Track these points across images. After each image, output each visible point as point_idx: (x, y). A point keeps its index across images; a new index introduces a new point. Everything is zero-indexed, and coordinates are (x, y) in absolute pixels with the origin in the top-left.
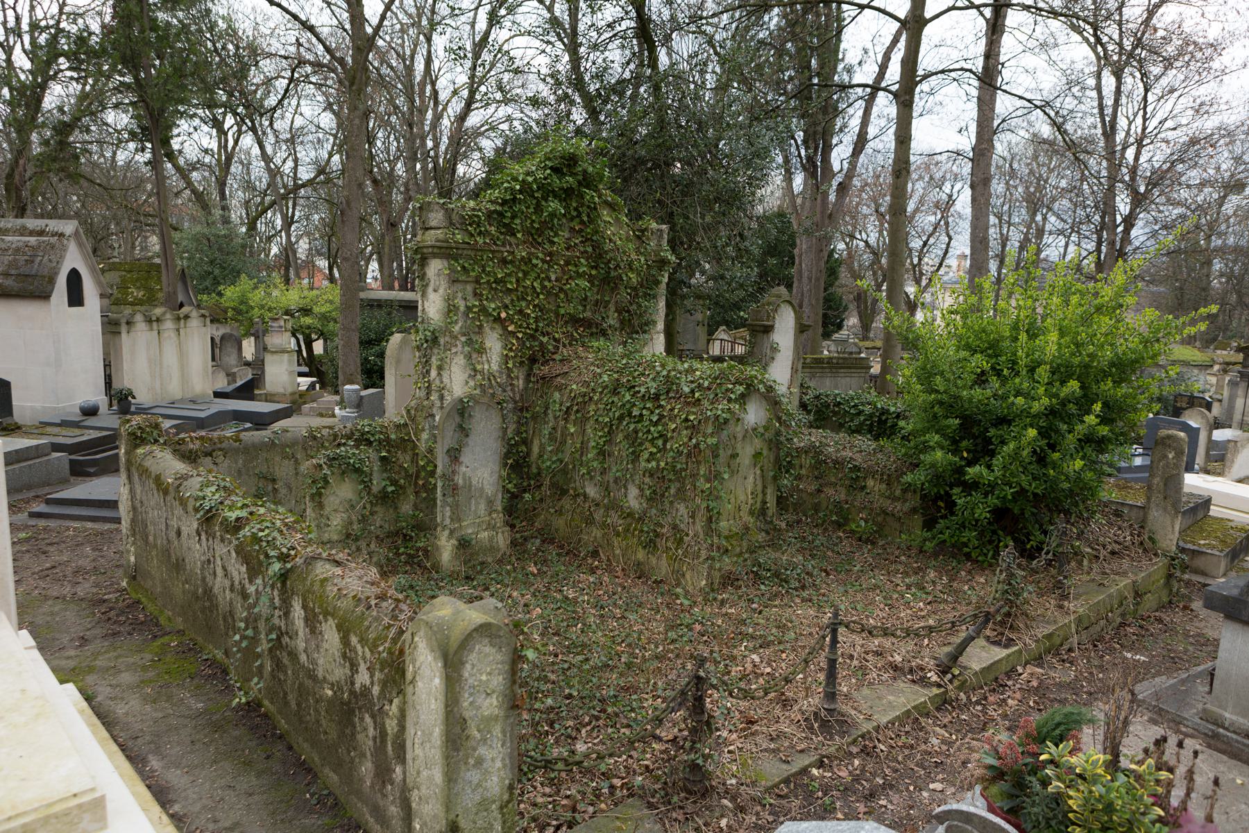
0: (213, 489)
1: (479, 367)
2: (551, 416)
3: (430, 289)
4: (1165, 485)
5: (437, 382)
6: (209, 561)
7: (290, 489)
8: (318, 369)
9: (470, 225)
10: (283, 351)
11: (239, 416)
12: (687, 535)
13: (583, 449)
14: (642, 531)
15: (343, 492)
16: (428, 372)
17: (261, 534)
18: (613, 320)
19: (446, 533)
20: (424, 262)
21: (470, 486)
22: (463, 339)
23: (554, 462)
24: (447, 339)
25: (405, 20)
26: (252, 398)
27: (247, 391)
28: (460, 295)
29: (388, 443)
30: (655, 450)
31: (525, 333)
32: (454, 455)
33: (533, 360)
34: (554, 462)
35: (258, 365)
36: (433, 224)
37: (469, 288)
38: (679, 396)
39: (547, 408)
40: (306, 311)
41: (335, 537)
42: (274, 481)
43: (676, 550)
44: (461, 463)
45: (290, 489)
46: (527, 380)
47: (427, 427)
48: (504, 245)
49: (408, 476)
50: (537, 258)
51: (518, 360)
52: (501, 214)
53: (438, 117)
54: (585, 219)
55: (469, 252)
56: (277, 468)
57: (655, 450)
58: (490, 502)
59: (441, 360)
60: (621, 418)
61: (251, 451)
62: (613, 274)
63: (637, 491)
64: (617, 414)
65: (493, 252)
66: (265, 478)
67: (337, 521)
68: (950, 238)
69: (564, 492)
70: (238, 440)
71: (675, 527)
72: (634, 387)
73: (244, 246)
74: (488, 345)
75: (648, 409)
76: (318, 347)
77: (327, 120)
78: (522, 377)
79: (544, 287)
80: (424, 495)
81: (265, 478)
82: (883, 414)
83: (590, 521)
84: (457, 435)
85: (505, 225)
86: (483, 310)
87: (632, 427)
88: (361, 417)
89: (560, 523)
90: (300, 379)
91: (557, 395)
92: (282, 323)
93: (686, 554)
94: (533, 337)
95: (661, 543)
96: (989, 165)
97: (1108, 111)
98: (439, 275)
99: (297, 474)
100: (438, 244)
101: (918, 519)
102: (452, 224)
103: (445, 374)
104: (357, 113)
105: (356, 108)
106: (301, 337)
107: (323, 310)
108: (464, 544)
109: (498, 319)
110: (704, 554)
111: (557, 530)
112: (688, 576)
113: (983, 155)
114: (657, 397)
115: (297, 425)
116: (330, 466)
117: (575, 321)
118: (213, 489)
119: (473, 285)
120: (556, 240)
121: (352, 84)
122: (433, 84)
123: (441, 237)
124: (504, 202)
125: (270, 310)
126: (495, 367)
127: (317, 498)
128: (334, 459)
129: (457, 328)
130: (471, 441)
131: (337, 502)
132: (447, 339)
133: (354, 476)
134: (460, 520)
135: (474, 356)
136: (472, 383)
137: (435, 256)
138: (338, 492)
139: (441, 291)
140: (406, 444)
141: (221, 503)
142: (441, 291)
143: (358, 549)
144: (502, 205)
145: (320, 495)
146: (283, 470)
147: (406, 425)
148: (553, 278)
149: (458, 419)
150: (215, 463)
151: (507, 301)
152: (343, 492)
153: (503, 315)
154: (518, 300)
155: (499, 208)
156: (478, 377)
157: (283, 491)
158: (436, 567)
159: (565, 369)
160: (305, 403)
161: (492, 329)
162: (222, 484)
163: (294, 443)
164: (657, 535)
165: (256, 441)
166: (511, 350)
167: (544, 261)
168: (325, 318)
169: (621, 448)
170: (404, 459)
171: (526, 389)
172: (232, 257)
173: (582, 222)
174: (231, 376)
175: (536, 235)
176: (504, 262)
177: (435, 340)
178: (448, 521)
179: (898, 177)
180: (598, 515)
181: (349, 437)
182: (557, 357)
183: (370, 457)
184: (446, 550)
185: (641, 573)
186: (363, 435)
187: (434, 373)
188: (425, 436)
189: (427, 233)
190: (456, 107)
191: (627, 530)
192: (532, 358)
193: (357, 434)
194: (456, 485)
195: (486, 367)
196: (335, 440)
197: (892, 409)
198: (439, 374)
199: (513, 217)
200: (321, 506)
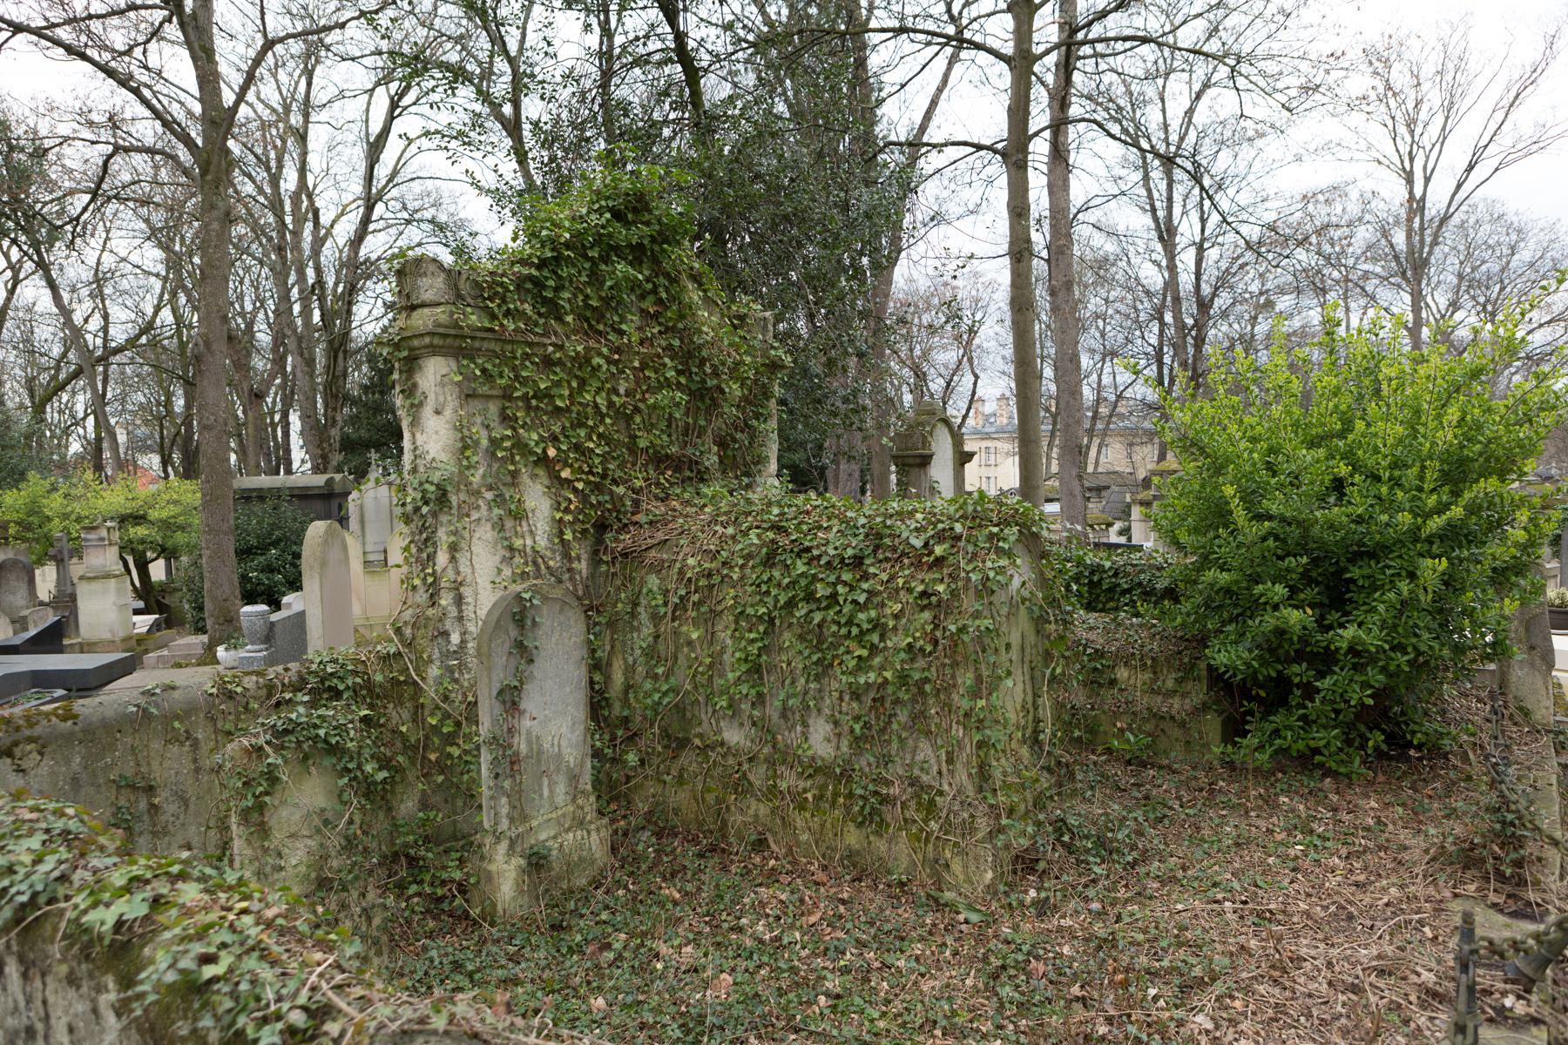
0: (35, 843)
1: (518, 543)
2: (644, 617)
3: (428, 411)
4: (1527, 630)
5: (451, 574)
6: (30, 1032)
7: (185, 802)
8: (158, 603)
9: (491, 299)
10: (107, 576)
11: (42, 680)
12: (941, 793)
13: (716, 665)
14: (850, 795)
15: (307, 796)
16: (431, 558)
17: (209, 971)
18: (711, 460)
19: (504, 846)
20: (412, 364)
21: (540, 752)
22: (489, 495)
23: (665, 694)
24: (463, 496)
25: (266, 114)
26: (60, 650)
27: (50, 640)
28: (479, 420)
30: (865, 653)
31: (587, 483)
32: (510, 699)
33: (602, 527)
34: (665, 694)
35: (66, 600)
36: (428, 296)
37: (493, 408)
38: (901, 554)
39: (636, 604)
40: (138, 519)
42: (150, 790)
43: (926, 821)
44: (522, 713)
45: (185, 802)
46: (595, 560)
47: (436, 655)
48: (546, 334)
49: (410, 748)
50: (600, 354)
51: (578, 527)
52: (539, 284)
53: (318, 243)
54: (664, 295)
55: (492, 346)
56: (155, 765)
57: (865, 653)
58: (574, 778)
59: (455, 533)
60: (791, 604)
61: (101, 735)
62: (710, 383)
63: (829, 727)
64: (782, 600)
65: (531, 345)
66: (133, 787)
67: (297, 857)
68: (977, 377)
69: (683, 743)
70: (69, 716)
71: (914, 781)
72: (808, 550)
73: (28, 437)
74: (530, 504)
75: (845, 583)
76: (157, 571)
77: (152, 257)
78: (584, 556)
79: (611, 404)
80: (440, 779)
81: (133, 787)
82: (1092, 573)
83: (741, 787)
84: (513, 662)
85: (546, 301)
86: (520, 446)
87: (818, 617)
88: (271, 661)
89: (680, 798)
90: (137, 618)
91: (653, 581)
92: (104, 533)
93: (947, 827)
94: (597, 488)
95: (892, 814)
96: (1070, 265)
97: (1161, 214)
98: (443, 385)
99: (197, 770)
100: (441, 330)
101: (1212, 724)
102: (459, 296)
103: (463, 559)
104: (215, 213)
105: (213, 207)
106: (130, 560)
107: (165, 514)
108: (536, 862)
109: (543, 460)
110: (983, 825)
111: (676, 812)
112: (956, 867)
113: (1062, 253)
114: (858, 561)
115: (124, 691)
116: (279, 749)
117: (659, 460)
118: (35, 843)
119: (499, 403)
120: (624, 327)
121: (204, 172)
122: (310, 196)
123: (443, 318)
124: (543, 264)
125: (79, 520)
126: (542, 542)
127: (255, 816)
128: (286, 732)
129: (476, 479)
130: (538, 669)
131: (297, 817)
132: (463, 496)
133: (328, 761)
134: (525, 818)
135: (509, 524)
136: (507, 572)
137: (434, 351)
139: (448, 412)
140: (403, 689)
141: (63, 878)
142: (448, 412)
143: (343, 906)
144: (538, 267)
145: (260, 807)
146: (168, 765)
148: (622, 391)
149: (514, 633)
150: (20, 770)
151: (556, 429)
152: (307, 796)
153: (552, 452)
154: (573, 427)
155: (534, 272)
156: (518, 560)
157: (172, 808)
158: (490, 917)
159: (660, 536)
160: (146, 651)
161: (534, 476)
162: (59, 825)
163: (189, 711)
164: (885, 800)
165: (109, 713)
166: (567, 511)
167: (609, 361)
168: (167, 525)
169: (791, 652)
170: (399, 718)
171: (592, 576)
172: (10, 453)
173: (660, 302)
174: (20, 623)
175: (592, 321)
176: (548, 363)
177: (442, 498)
178: (504, 824)
179: (1019, 261)
180: (758, 776)
181: (297, 689)
182: (641, 518)
183: (340, 716)
184: (505, 876)
185: (861, 870)
187: (442, 558)
188: (434, 671)
189: (415, 314)
190: (345, 230)
191: (819, 798)
192: (599, 525)
194: (517, 754)
195: (529, 542)
196: (269, 696)
197: (1108, 564)
198: (453, 559)
199: (557, 289)
200: (263, 831)
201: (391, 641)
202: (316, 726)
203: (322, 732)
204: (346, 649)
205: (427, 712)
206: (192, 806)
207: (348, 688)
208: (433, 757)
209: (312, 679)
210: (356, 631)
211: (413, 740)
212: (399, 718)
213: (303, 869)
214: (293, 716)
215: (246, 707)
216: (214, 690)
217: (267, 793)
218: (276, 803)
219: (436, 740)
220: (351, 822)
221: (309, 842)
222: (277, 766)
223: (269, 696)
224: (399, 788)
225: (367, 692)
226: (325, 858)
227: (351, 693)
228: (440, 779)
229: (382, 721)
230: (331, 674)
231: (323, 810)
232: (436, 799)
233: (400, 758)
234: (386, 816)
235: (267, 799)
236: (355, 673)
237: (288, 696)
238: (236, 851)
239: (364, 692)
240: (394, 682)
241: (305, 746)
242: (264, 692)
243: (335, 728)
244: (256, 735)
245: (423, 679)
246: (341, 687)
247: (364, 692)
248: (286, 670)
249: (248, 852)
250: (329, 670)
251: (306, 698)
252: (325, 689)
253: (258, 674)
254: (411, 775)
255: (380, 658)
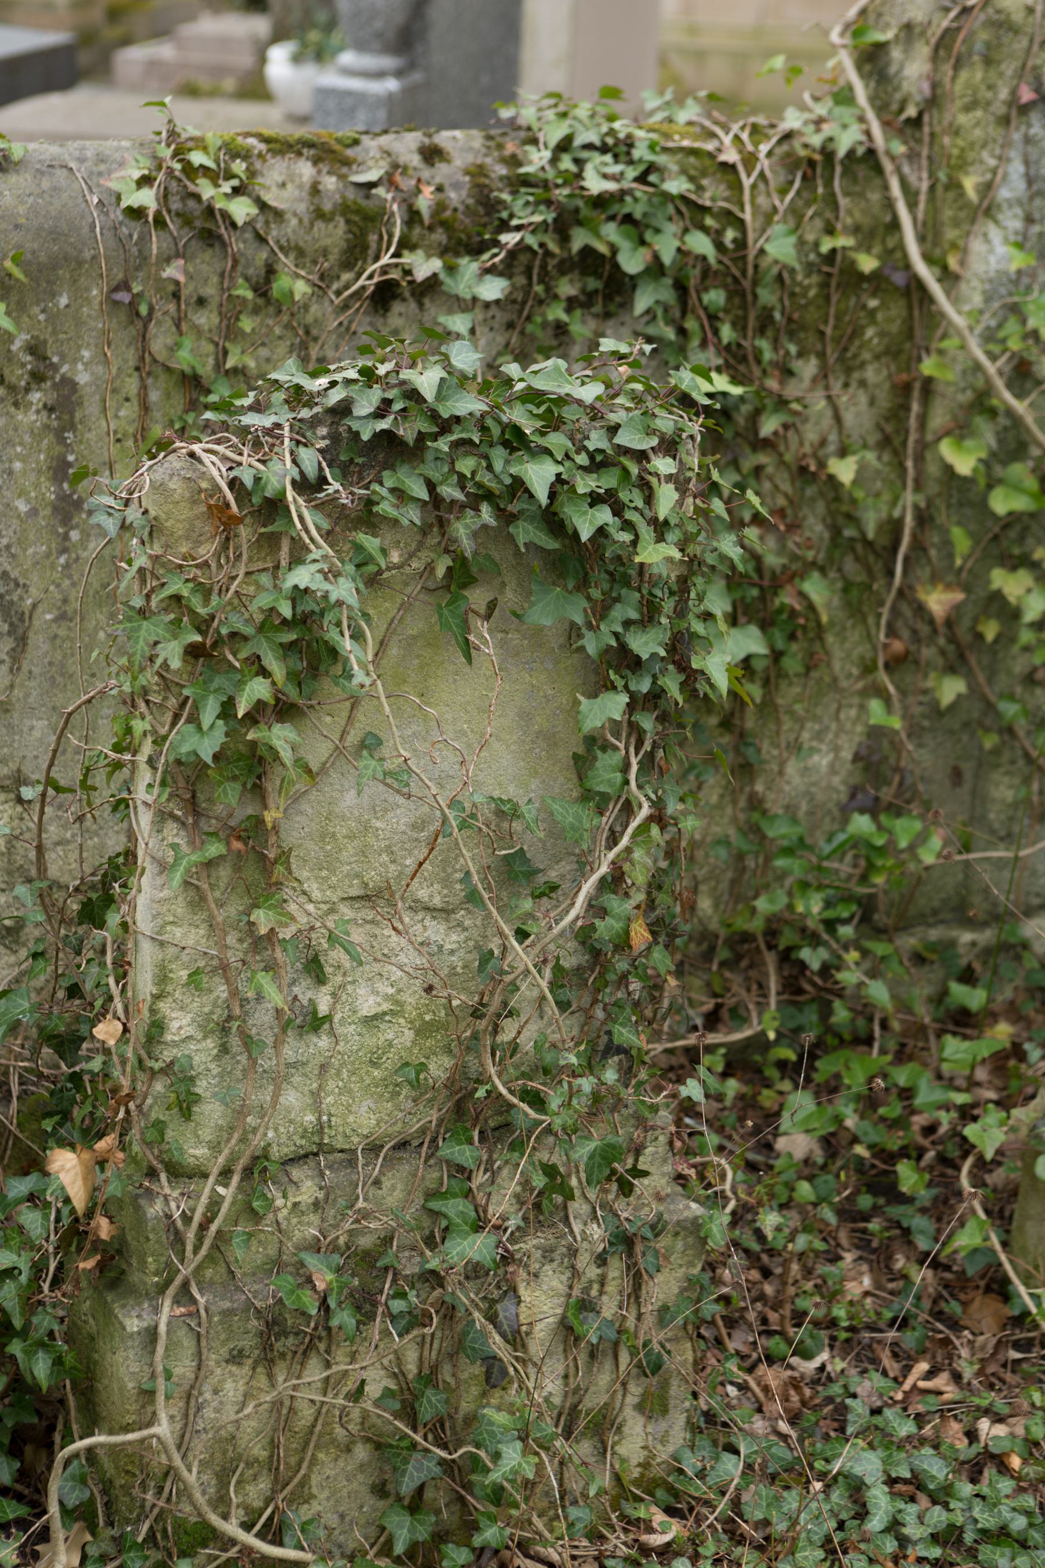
29: (740, 295)
41: (363, 1116)
47: (1012, 187)
49: (870, 558)
127: (228, 799)
128: (390, 448)
131: (400, 817)
133: (553, 609)
138: (400, 746)
145: (253, 767)
147: (868, 159)
160: (126, 41)
170: (831, 414)
181: (468, 233)
186: (562, 227)
193: (527, 214)
196: (356, 253)
200: (256, 860)
201: (844, 97)
202: (515, 441)
203: (539, 476)
204: (660, 116)
205: (939, 418)
206: (38, 642)
207: (656, 269)
208: (938, 601)
209: (527, 214)
210: (663, 62)
211: (871, 522)
212: (831, 414)
213: (400, 1036)
214: (427, 380)
215: (262, 288)
216: (147, 198)
217: (284, 710)
218: (318, 753)
219: (961, 541)
220: (615, 882)
221: (435, 931)
222: (326, 606)
223: (356, 253)
224: (788, 694)
225: (727, 300)
226: (487, 1013)
227: (665, 292)
228: (951, 689)
229: (769, 426)
230: (600, 202)
231: (506, 812)
232: (923, 759)
233: (817, 590)
234: (731, 794)
235: (280, 736)
236: (691, 211)
237: (424, 266)
238: (143, 922)
239: (715, 297)
240: (836, 274)
241: (462, 530)
242: (334, 235)
243: (598, 463)
244: (262, 443)
245: (948, 277)
246: (632, 262)
247: (715, 297)
248: (432, 154)
249: (190, 936)
250: (595, 184)
251: (493, 289)
252: (569, 268)
253: (329, 154)
254: (843, 653)
255: (791, 163)
